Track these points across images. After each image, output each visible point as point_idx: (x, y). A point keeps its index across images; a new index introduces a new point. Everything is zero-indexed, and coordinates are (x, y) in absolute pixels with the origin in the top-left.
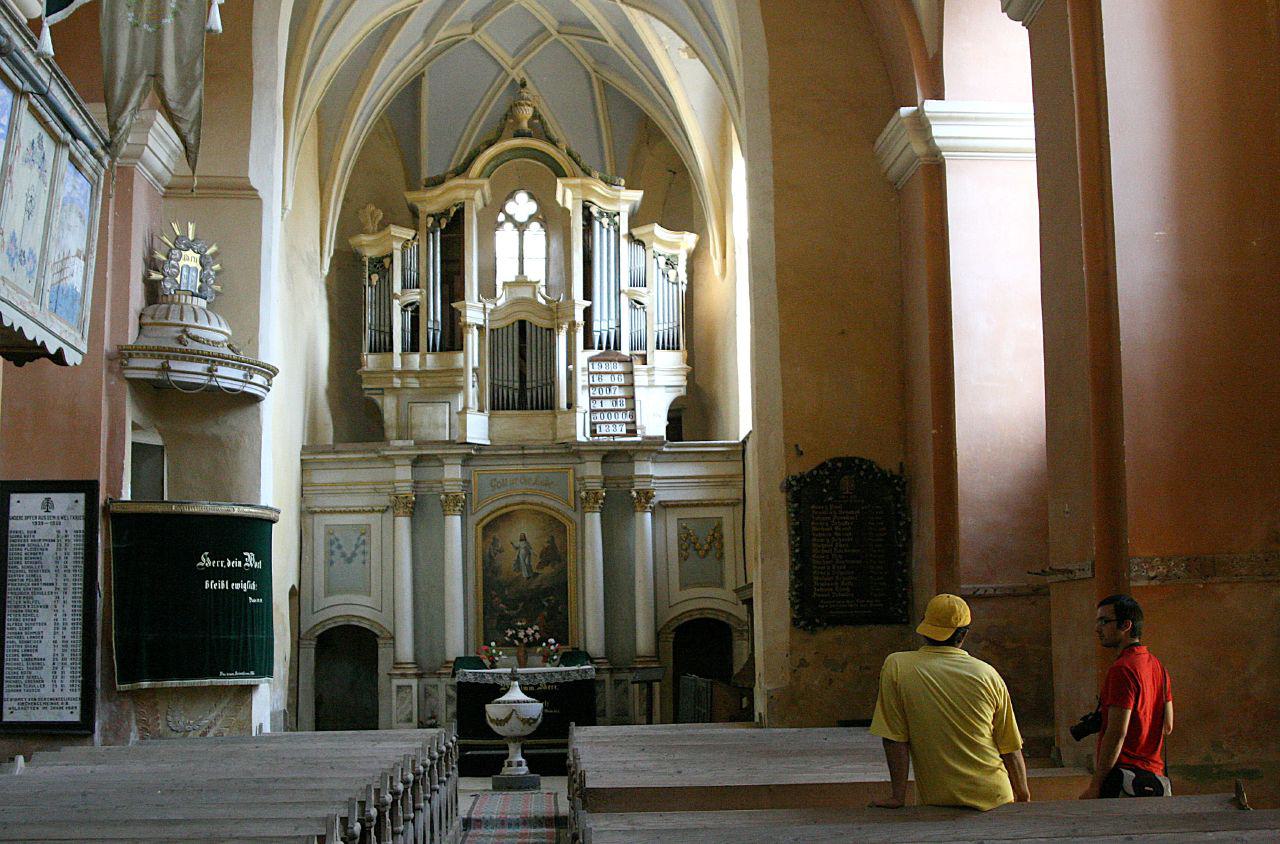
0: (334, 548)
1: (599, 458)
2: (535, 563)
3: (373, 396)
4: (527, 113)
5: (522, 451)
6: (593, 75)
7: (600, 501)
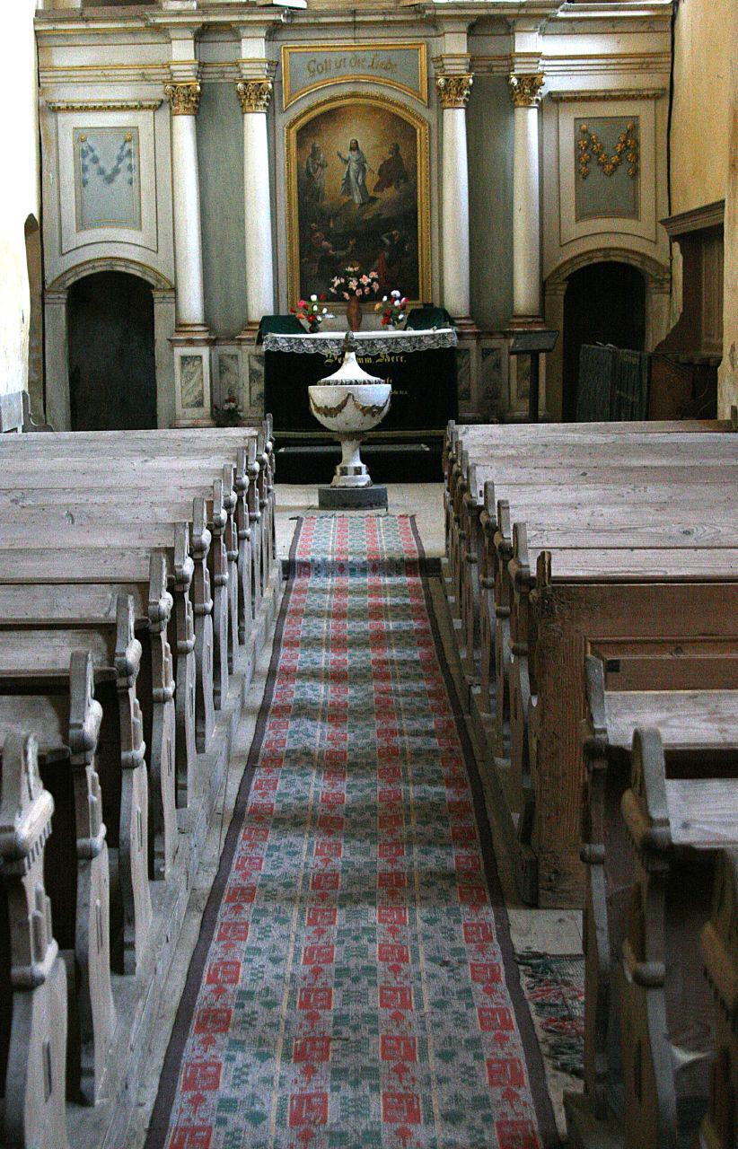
0: (87, 162)
1: (464, 27)
2: (372, 180)
7: (465, 92)
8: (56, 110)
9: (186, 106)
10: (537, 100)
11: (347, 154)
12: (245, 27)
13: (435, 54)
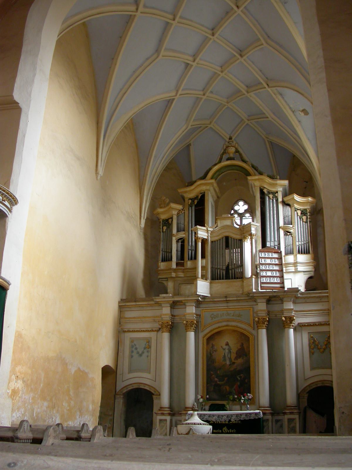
0: (133, 349)
1: (265, 300)
2: (233, 356)
3: (163, 282)
4: (232, 150)
5: (226, 299)
6: (266, 140)
7: (266, 323)
8: (125, 332)
9: (166, 329)
10: (293, 326)
11: (225, 347)
12: (187, 302)
13: (255, 310)
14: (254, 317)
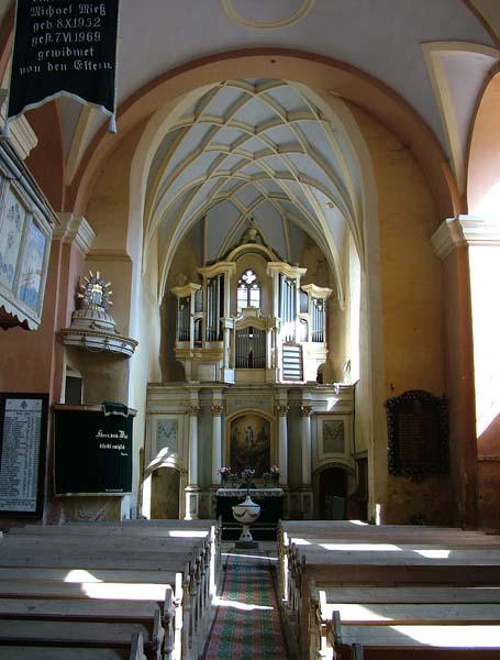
2: (255, 439)
5: (250, 387)
14: (275, 407)
